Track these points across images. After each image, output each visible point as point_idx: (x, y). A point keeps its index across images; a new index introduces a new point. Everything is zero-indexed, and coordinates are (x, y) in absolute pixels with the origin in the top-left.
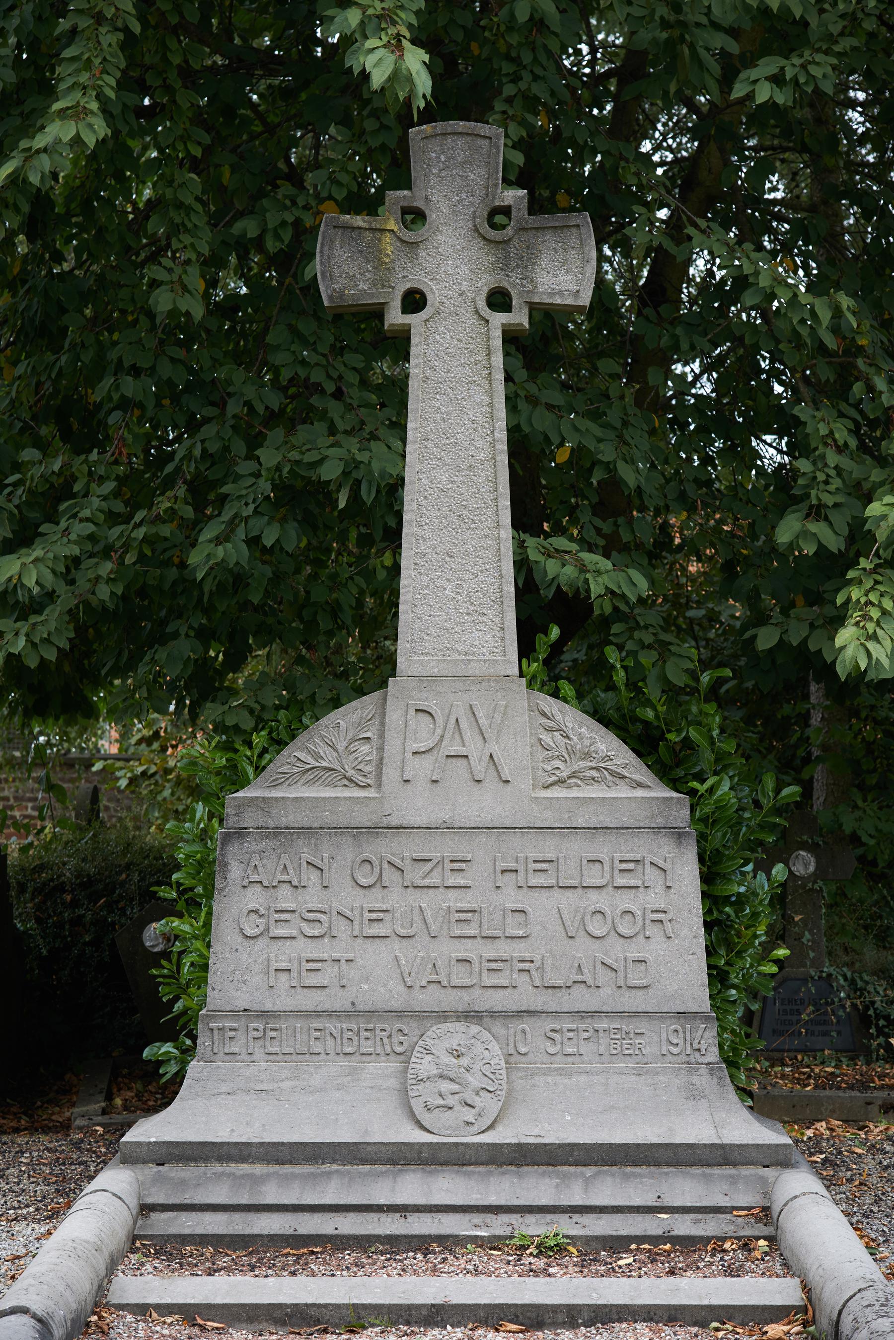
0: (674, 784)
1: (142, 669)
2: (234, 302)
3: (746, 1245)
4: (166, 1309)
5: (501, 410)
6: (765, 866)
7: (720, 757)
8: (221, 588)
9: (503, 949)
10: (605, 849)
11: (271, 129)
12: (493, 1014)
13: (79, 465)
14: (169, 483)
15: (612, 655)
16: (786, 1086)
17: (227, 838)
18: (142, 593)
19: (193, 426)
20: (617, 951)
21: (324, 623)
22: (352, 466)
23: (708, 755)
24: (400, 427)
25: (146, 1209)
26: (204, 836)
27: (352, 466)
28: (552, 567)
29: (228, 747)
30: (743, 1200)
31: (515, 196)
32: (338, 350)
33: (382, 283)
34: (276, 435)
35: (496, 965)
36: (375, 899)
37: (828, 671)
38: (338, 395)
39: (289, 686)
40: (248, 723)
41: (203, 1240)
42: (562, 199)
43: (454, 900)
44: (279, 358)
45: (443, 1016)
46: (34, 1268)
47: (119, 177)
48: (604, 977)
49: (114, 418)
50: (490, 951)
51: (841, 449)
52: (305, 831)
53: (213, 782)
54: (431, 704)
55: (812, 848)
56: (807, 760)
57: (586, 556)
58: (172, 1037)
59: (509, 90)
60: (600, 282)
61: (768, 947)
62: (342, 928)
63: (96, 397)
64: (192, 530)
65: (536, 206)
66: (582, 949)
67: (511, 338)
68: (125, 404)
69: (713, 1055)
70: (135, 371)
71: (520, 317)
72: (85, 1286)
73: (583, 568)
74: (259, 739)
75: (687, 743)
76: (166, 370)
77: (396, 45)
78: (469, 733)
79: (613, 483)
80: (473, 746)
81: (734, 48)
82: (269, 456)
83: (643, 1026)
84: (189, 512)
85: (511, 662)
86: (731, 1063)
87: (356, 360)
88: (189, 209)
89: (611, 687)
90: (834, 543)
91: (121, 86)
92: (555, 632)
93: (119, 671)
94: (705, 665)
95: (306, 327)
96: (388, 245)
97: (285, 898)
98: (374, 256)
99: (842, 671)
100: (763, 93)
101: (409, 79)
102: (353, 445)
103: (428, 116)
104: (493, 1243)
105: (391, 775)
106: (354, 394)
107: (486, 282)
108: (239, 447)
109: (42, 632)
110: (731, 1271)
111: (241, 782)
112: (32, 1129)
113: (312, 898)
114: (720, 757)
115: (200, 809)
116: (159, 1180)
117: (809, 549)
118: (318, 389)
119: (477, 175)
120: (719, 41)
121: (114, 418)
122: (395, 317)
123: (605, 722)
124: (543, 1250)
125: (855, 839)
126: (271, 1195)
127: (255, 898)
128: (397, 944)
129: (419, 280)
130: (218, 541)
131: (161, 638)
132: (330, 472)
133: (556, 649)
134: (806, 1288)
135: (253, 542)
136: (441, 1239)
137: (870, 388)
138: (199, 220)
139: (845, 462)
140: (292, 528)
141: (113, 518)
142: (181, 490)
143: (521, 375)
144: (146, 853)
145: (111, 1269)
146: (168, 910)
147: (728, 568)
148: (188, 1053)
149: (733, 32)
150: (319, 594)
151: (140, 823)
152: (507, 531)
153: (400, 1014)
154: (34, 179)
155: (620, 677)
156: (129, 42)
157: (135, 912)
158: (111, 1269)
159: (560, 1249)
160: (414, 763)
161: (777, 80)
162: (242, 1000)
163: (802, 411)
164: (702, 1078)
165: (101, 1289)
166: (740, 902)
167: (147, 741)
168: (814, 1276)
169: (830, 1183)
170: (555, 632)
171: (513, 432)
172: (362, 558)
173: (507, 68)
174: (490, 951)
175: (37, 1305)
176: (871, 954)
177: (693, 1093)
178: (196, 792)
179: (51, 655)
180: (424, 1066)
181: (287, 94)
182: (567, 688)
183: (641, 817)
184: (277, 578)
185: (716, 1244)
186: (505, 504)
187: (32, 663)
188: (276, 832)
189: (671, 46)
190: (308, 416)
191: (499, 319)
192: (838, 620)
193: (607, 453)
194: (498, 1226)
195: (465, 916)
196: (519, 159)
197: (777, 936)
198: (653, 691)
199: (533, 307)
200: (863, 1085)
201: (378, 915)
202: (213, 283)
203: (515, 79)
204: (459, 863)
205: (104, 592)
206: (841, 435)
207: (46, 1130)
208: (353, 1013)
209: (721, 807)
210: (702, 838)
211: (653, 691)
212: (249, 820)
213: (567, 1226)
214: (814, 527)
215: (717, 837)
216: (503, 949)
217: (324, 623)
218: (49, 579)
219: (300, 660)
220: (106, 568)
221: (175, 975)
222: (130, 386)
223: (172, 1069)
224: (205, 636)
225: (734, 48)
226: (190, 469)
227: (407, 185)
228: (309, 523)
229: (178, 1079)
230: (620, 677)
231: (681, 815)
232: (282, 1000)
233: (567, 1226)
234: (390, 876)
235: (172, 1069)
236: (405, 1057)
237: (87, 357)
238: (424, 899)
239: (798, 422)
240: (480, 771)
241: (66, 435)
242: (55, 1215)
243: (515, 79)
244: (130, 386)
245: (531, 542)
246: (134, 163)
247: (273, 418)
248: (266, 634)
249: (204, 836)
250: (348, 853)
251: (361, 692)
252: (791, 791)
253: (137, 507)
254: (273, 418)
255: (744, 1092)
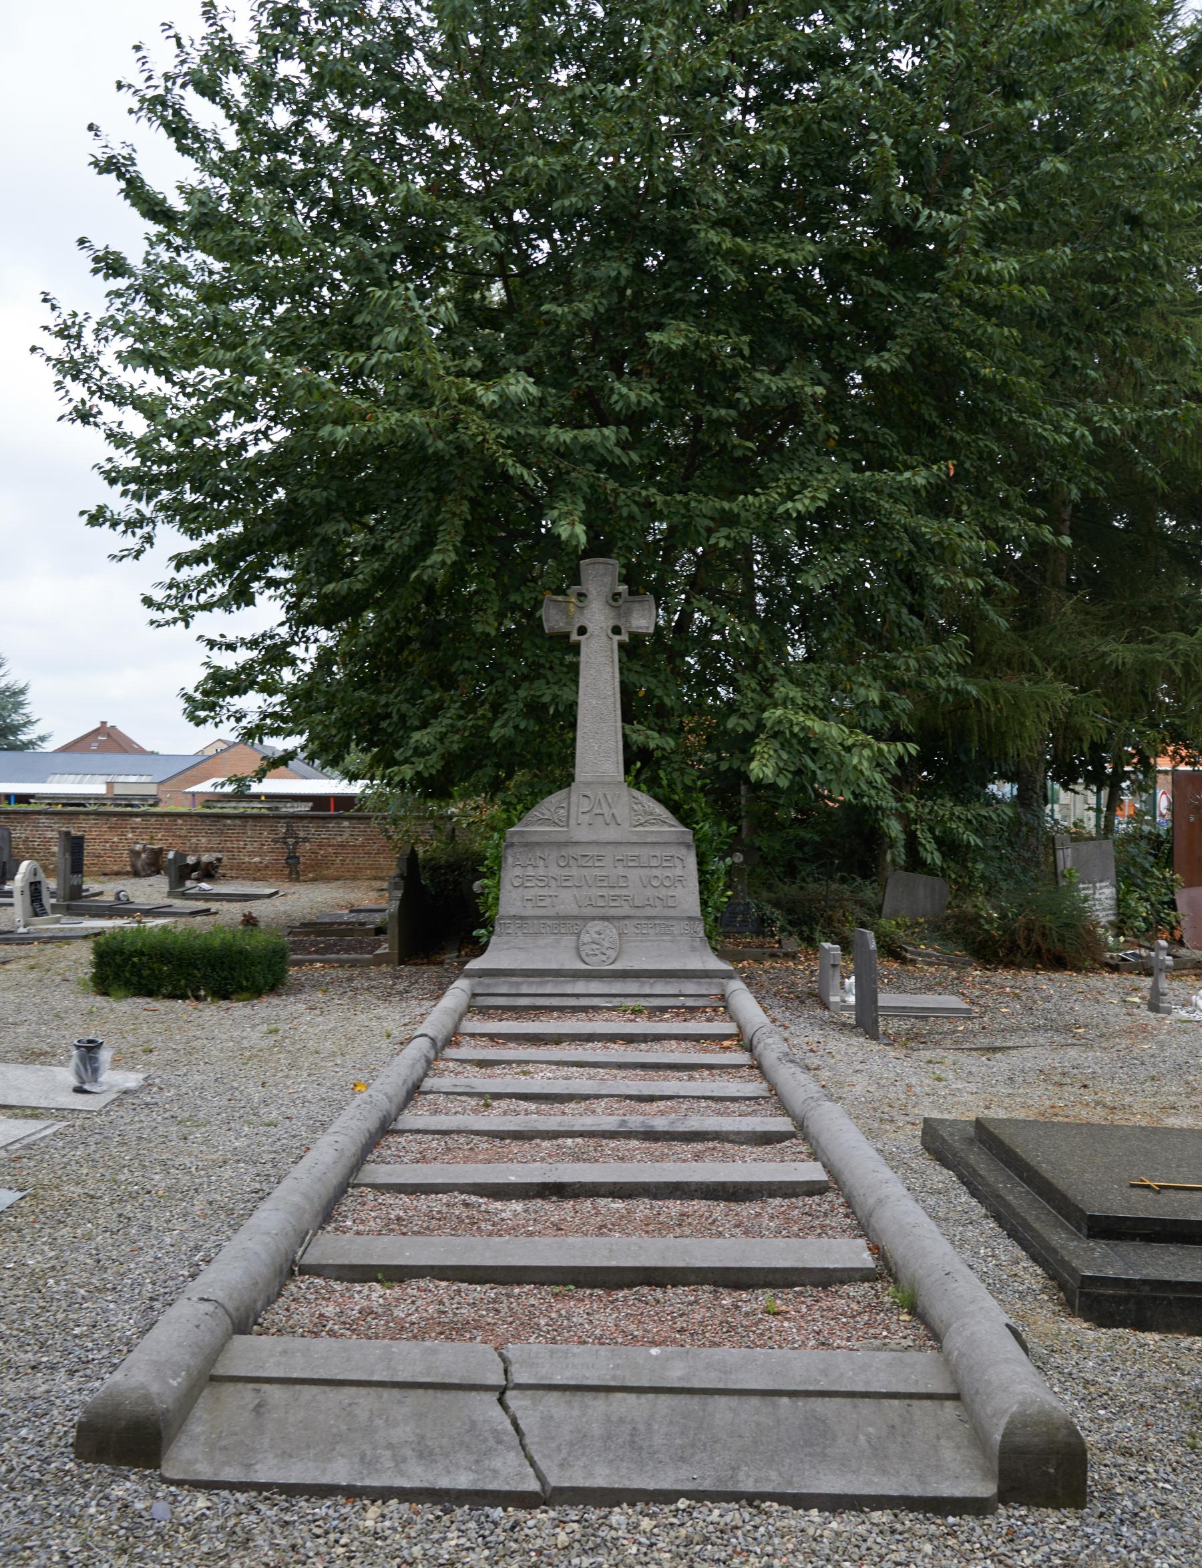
0: (686, 825)
1: (472, 780)
2: (509, 632)
3: (715, 1010)
4: (482, 1035)
5: (617, 675)
6: (722, 859)
7: (705, 815)
8: (504, 747)
9: (618, 892)
10: (658, 852)
11: (524, 562)
12: (613, 918)
13: (446, 697)
14: (482, 704)
15: (662, 774)
16: (731, 947)
17: (507, 847)
18: (472, 749)
19: (492, 681)
20: (663, 892)
21: (546, 761)
22: (555, 697)
23: (700, 814)
24: (576, 682)
25: (474, 995)
26: (498, 846)
27: (555, 697)
28: (634, 737)
29: (507, 810)
30: (714, 992)
31: (623, 588)
32: (551, 650)
33: (569, 623)
34: (526, 684)
35: (615, 898)
36: (566, 872)
37: (747, 779)
38: (551, 668)
39: (532, 786)
40: (515, 801)
41: (497, 1008)
42: (641, 590)
43: (598, 872)
44: (527, 654)
45: (594, 918)
46: (429, 1018)
47: (462, 580)
48: (658, 903)
49: (461, 677)
50: (612, 892)
51: (753, 691)
52: (538, 844)
53: (501, 825)
54: (589, 793)
55: (741, 852)
56: (740, 817)
57: (650, 732)
58: (483, 926)
59: (620, 544)
60: (657, 625)
61: (724, 891)
62: (553, 883)
63: (453, 669)
64: (492, 722)
65: (631, 593)
66: (649, 892)
67: (621, 646)
68: (465, 672)
69: (702, 934)
70: (469, 659)
71: (625, 637)
72: (450, 1026)
73: (647, 737)
74: (519, 807)
75: (692, 809)
76: (482, 659)
77: (573, 524)
78: (604, 805)
79: (662, 705)
80: (605, 810)
81: (712, 524)
82: (522, 693)
83: (674, 922)
84: (490, 715)
85: (621, 777)
86: (709, 938)
87: (558, 654)
88: (489, 593)
89: (660, 786)
90: (750, 728)
91: (462, 542)
92: (639, 764)
93: (462, 780)
94: (699, 778)
95: (538, 641)
96: (572, 608)
97: (530, 871)
98: (566, 613)
99: (753, 779)
100: (722, 543)
101: (577, 536)
102: (556, 688)
103: (587, 554)
104: (614, 1009)
105: (572, 822)
106: (557, 668)
107: (611, 623)
108: (511, 689)
109: (430, 763)
110: (709, 1020)
111: (512, 825)
112: (429, 964)
113: (541, 871)
114: (705, 815)
115: (496, 836)
116: (480, 984)
117: (741, 731)
118: (543, 666)
119: (608, 580)
120: (707, 522)
121: (461, 677)
122: (574, 637)
123: (659, 800)
124: (633, 1012)
125: (759, 849)
126: (525, 990)
127: (518, 871)
128: (575, 890)
129: (584, 622)
130: (503, 726)
131: (480, 766)
132: (546, 699)
133: (639, 771)
134: (739, 1027)
135: (516, 727)
136: (593, 1007)
137: (765, 667)
138: (494, 597)
139: (755, 696)
140: (532, 722)
141: (461, 717)
142: (487, 706)
143: (625, 659)
144: (474, 853)
145: (460, 1019)
146: (482, 876)
147: (708, 739)
148: (491, 933)
149: (712, 519)
150: (544, 750)
151: (472, 841)
152: (619, 724)
153: (576, 917)
154: (425, 578)
155: (665, 782)
156: (467, 524)
157: (469, 877)
158: (460, 1019)
159: (641, 1012)
160: (581, 817)
161: (728, 538)
162: (513, 912)
163: (738, 676)
164: (697, 944)
165: (457, 1027)
166: (713, 873)
167: (475, 809)
168: (742, 1021)
169: (749, 985)
170: (639, 764)
171: (622, 682)
172: (560, 735)
173: (619, 535)
174: (612, 892)
175: (431, 1034)
176: (765, 894)
177: (694, 949)
178: (494, 829)
179: (434, 772)
180: (586, 938)
181: (531, 547)
182: (643, 787)
183: (672, 838)
184: (527, 743)
185: (703, 1009)
186: (619, 712)
187: (426, 775)
188: (527, 845)
189: (687, 525)
190: (539, 676)
191: (617, 638)
192: (752, 759)
193: (659, 692)
194: (615, 1002)
195: (603, 878)
196: (624, 571)
197: (728, 887)
198: (679, 788)
199: (630, 633)
200: (762, 946)
201: (568, 878)
202: (501, 624)
203: (623, 539)
204: (600, 857)
205: (455, 747)
206: (753, 685)
207: (435, 964)
208: (557, 917)
209: (705, 835)
210: (698, 847)
211: (679, 788)
212: (515, 839)
213: (643, 1002)
214: (742, 722)
215: (704, 847)
216: (618, 892)
217: (546, 761)
218: (432, 741)
219: (536, 775)
220: (456, 737)
221: (486, 902)
222: (466, 664)
223: (484, 940)
224: (498, 766)
225: (712, 524)
226: (491, 698)
227: (578, 583)
228: (539, 721)
229: (487, 944)
230: (665, 782)
231: (689, 838)
232: (529, 912)
233: (643, 1002)
234: (572, 862)
235: (484, 940)
236: (578, 935)
237: (450, 653)
238: (585, 872)
239: (736, 680)
240: (608, 819)
241: (442, 685)
242: (438, 997)
243: (623, 539)
244: (466, 664)
245: (627, 726)
246: (468, 575)
247: (525, 678)
248: (522, 765)
249: (498, 846)
250: (555, 853)
251: (560, 788)
252: (733, 828)
253: (468, 713)
254: (525, 678)
255: (714, 949)
